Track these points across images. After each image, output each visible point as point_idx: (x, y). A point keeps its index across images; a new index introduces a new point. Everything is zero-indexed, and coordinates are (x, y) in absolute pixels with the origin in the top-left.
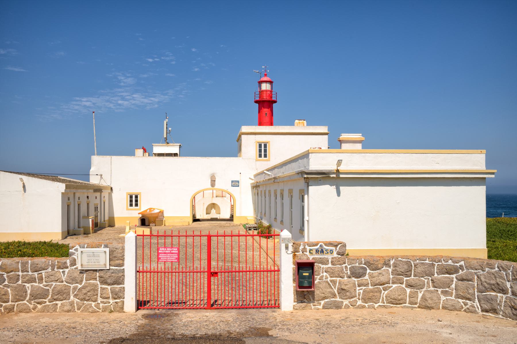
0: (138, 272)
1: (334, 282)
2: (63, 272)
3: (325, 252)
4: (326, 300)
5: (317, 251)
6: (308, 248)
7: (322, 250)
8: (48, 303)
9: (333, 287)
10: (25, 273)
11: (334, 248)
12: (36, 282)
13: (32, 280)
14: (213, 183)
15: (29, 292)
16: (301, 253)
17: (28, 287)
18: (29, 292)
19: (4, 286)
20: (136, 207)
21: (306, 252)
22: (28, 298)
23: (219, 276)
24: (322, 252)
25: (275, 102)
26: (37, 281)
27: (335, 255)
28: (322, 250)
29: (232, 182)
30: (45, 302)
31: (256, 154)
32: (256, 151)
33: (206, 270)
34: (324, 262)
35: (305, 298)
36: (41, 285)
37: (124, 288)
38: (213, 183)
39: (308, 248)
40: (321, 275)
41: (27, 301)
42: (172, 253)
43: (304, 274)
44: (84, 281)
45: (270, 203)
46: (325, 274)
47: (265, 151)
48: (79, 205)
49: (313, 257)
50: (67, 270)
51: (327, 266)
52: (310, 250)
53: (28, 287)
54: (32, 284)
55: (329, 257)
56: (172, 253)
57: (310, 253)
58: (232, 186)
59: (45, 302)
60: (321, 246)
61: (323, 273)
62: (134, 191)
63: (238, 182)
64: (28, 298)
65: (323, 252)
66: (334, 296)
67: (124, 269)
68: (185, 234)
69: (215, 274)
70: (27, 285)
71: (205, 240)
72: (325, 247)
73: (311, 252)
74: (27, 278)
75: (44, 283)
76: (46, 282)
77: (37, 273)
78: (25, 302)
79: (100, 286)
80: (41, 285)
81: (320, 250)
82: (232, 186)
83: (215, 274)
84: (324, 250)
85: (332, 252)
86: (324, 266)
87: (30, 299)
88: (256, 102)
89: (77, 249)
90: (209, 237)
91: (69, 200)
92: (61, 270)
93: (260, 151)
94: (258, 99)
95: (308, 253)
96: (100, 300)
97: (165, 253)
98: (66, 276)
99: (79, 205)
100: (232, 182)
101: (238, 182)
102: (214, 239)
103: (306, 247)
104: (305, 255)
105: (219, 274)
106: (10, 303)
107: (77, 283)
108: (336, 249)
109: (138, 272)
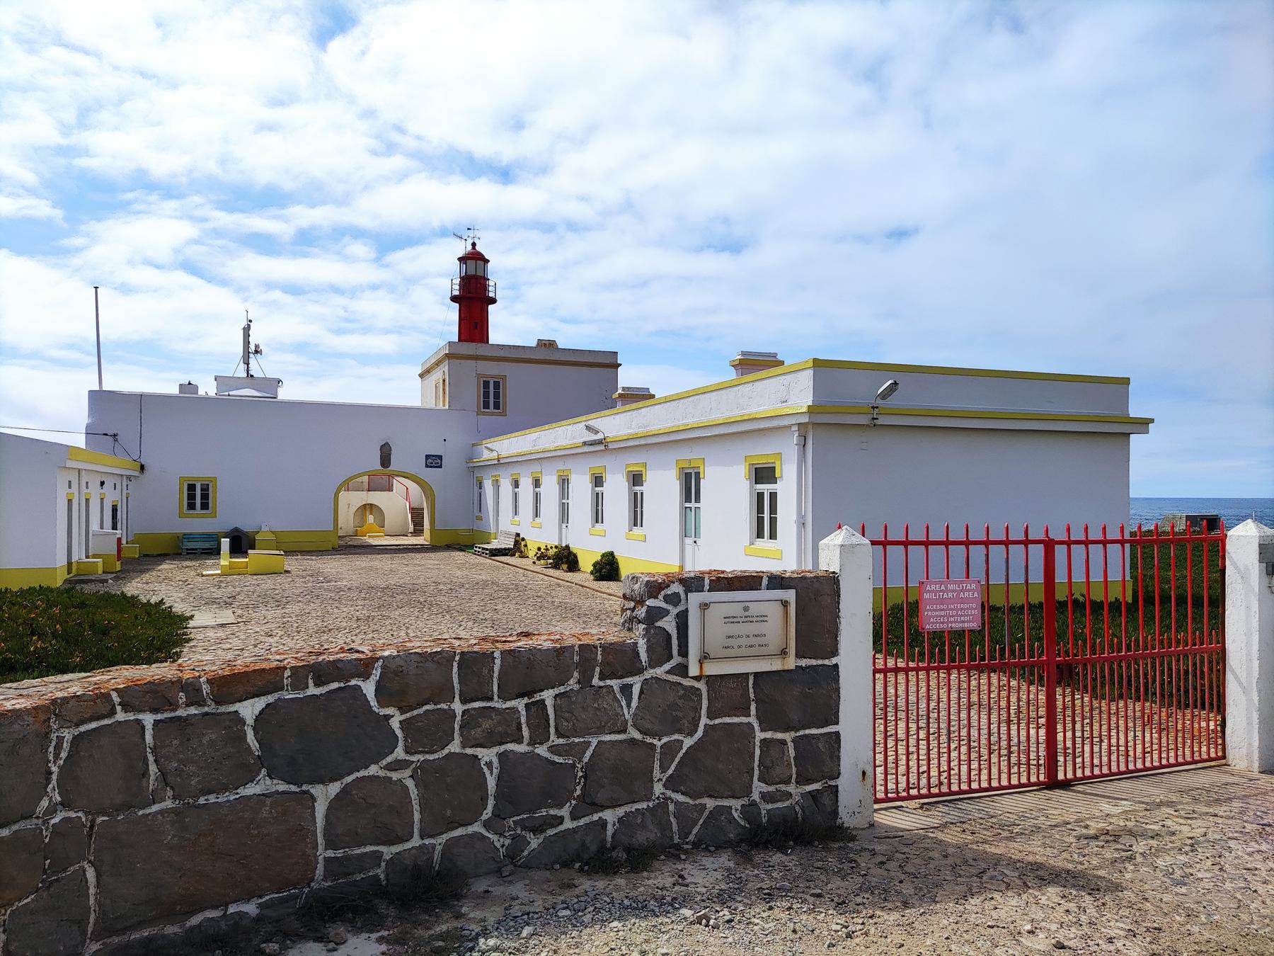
0: (879, 671)
2: (627, 689)
8: (568, 824)
10: (477, 705)
12: (519, 740)
13: (506, 730)
15: (491, 783)
17: (489, 765)
18: (491, 783)
19: (389, 767)
22: (487, 813)
25: (493, 301)
26: (526, 732)
29: (428, 457)
30: (561, 820)
32: (479, 396)
36: (542, 750)
37: (837, 734)
41: (486, 825)
44: (704, 721)
47: (497, 395)
50: (636, 682)
53: (489, 765)
54: (502, 748)
59: (561, 820)
62: (198, 471)
64: (487, 813)
67: (836, 666)
68: (1100, 537)
70: (487, 755)
74: (486, 724)
75: (554, 739)
76: (559, 734)
77: (526, 700)
78: (477, 828)
79: (760, 735)
80: (542, 750)
87: (497, 814)
88: (454, 299)
89: (677, 595)
90: (1049, 545)
92: (615, 683)
93: (486, 395)
94: (456, 293)
96: (758, 787)
98: (634, 704)
99: (87, 500)
100: (428, 457)
101: (440, 457)
102: (1060, 551)
106: (416, 841)
107: (680, 731)
109: (879, 671)
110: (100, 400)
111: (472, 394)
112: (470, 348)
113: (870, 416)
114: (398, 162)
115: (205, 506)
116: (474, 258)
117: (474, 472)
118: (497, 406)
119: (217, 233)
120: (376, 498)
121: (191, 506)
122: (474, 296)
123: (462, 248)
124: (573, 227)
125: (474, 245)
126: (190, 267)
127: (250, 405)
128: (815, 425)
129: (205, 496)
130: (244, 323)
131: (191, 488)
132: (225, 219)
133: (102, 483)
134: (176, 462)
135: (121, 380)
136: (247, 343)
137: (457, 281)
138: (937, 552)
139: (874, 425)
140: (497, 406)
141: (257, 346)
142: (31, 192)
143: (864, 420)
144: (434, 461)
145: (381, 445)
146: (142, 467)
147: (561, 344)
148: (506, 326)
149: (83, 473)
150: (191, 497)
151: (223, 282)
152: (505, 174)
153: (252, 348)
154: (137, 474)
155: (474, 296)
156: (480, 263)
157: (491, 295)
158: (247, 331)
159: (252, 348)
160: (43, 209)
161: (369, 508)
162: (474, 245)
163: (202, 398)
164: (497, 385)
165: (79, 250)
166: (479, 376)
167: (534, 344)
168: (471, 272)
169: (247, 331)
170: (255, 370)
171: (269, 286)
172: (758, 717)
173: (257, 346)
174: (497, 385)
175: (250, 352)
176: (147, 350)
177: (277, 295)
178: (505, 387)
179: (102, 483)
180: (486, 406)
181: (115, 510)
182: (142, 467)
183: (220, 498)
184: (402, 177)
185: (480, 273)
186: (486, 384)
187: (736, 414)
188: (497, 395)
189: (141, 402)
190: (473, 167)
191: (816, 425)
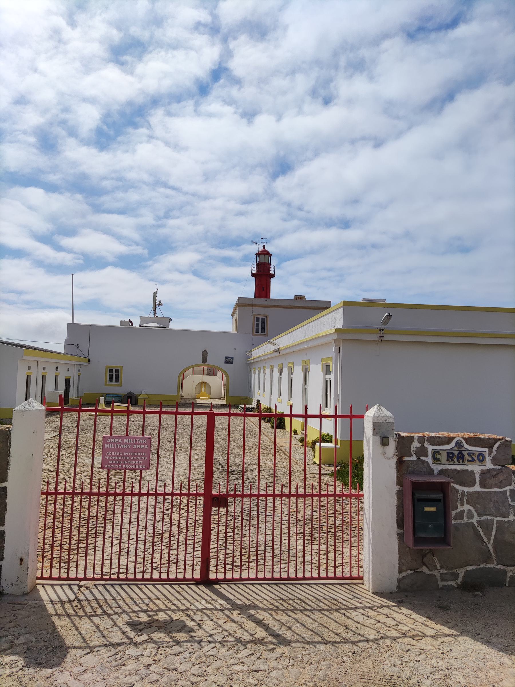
1: (487, 526)
3: (467, 457)
4: (469, 568)
5: (450, 456)
6: (430, 448)
7: (460, 452)
9: (485, 540)
11: (486, 450)
14: (204, 359)
16: (414, 458)
20: (116, 383)
21: (427, 456)
23: (231, 508)
24: (461, 457)
25: (273, 276)
27: (489, 465)
28: (460, 452)
29: (226, 358)
31: (253, 329)
33: (201, 490)
34: (466, 478)
35: (424, 564)
38: (204, 359)
39: (430, 448)
40: (460, 508)
42: (135, 450)
43: (427, 509)
45: (271, 380)
46: (466, 507)
47: (263, 325)
48: (44, 377)
49: (440, 467)
51: (471, 490)
52: (435, 453)
55: (476, 469)
56: (135, 450)
57: (434, 458)
58: (225, 363)
60: (458, 444)
61: (462, 505)
62: (115, 363)
63: (232, 358)
65: (463, 458)
66: (488, 558)
69: (221, 501)
71: (201, 421)
72: (466, 446)
73: (438, 456)
81: (456, 453)
82: (225, 363)
83: (221, 501)
84: (465, 453)
85: (482, 460)
86: (466, 489)
88: (253, 275)
91: (29, 368)
93: (257, 325)
94: (254, 272)
95: (429, 459)
97: (119, 450)
99: (44, 377)
100: (226, 358)
101: (232, 358)
103: (426, 444)
104: (423, 462)
105: (230, 499)
108: (490, 452)
110: (72, 328)
111: (250, 325)
112: (262, 301)
113: (379, 335)
114: (295, 222)
115: (117, 381)
116: (264, 254)
117: (249, 365)
118: (263, 331)
119: (210, 257)
120: (208, 379)
121: (111, 380)
122: (263, 275)
123: (257, 248)
124: (374, 246)
125: (264, 247)
126: (196, 273)
127: (157, 329)
128: (345, 340)
129: (117, 376)
130: (154, 291)
131: (111, 371)
132: (215, 252)
133: (57, 368)
134: (104, 358)
135: (84, 318)
136: (155, 300)
137: (255, 266)
138: (247, 492)
139: (381, 340)
140: (263, 331)
141: (160, 302)
142: (137, 244)
143: (375, 337)
144: (229, 360)
145: (205, 352)
146: (89, 361)
147: (308, 298)
148: (278, 290)
149: (39, 363)
150: (111, 376)
151: (206, 278)
152: (345, 224)
153: (158, 303)
154: (86, 364)
155: (263, 275)
156: (267, 256)
157: (272, 272)
158: (155, 294)
159: (158, 303)
160: (139, 250)
161: (203, 384)
162: (264, 247)
163: (171, 330)
164: (263, 320)
165: (150, 266)
166: (254, 315)
167: (292, 298)
168: (262, 261)
169: (155, 294)
170: (159, 314)
171: (226, 279)
172: (478, 493)
173: (160, 302)
174: (263, 320)
175: (156, 304)
176: (94, 305)
177: (228, 283)
178: (267, 321)
179: (57, 368)
180: (257, 331)
181: (67, 382)
182: (89, 361)
183: (124, 377)
184: (296, 229)
185: (266, 261)
186: (258, 319)
187: (314, 335)
188: (263, 325)
189: (90, 330)
190: (330, 223)
191: (345, 340)
